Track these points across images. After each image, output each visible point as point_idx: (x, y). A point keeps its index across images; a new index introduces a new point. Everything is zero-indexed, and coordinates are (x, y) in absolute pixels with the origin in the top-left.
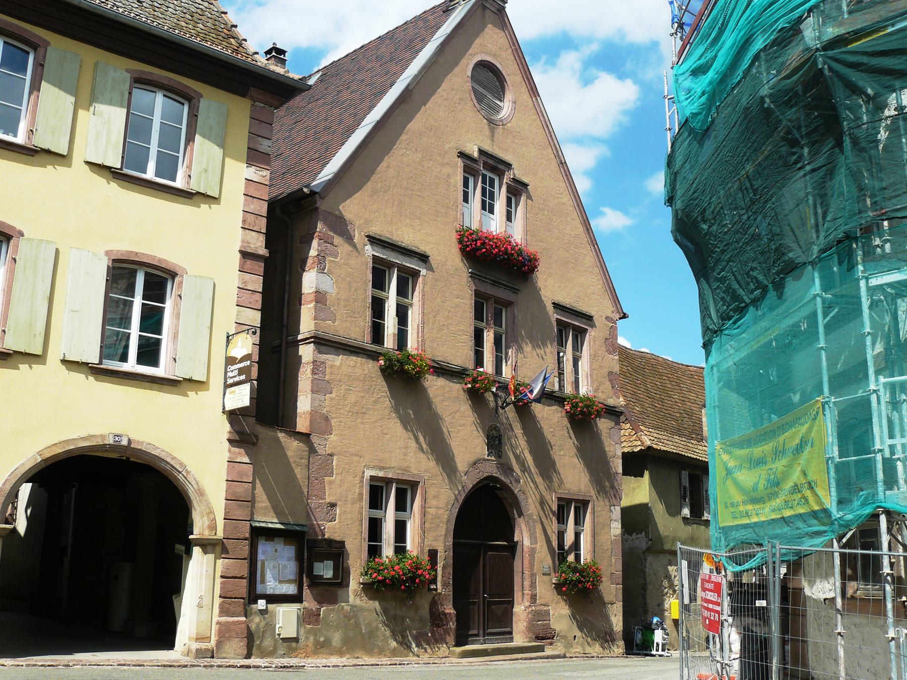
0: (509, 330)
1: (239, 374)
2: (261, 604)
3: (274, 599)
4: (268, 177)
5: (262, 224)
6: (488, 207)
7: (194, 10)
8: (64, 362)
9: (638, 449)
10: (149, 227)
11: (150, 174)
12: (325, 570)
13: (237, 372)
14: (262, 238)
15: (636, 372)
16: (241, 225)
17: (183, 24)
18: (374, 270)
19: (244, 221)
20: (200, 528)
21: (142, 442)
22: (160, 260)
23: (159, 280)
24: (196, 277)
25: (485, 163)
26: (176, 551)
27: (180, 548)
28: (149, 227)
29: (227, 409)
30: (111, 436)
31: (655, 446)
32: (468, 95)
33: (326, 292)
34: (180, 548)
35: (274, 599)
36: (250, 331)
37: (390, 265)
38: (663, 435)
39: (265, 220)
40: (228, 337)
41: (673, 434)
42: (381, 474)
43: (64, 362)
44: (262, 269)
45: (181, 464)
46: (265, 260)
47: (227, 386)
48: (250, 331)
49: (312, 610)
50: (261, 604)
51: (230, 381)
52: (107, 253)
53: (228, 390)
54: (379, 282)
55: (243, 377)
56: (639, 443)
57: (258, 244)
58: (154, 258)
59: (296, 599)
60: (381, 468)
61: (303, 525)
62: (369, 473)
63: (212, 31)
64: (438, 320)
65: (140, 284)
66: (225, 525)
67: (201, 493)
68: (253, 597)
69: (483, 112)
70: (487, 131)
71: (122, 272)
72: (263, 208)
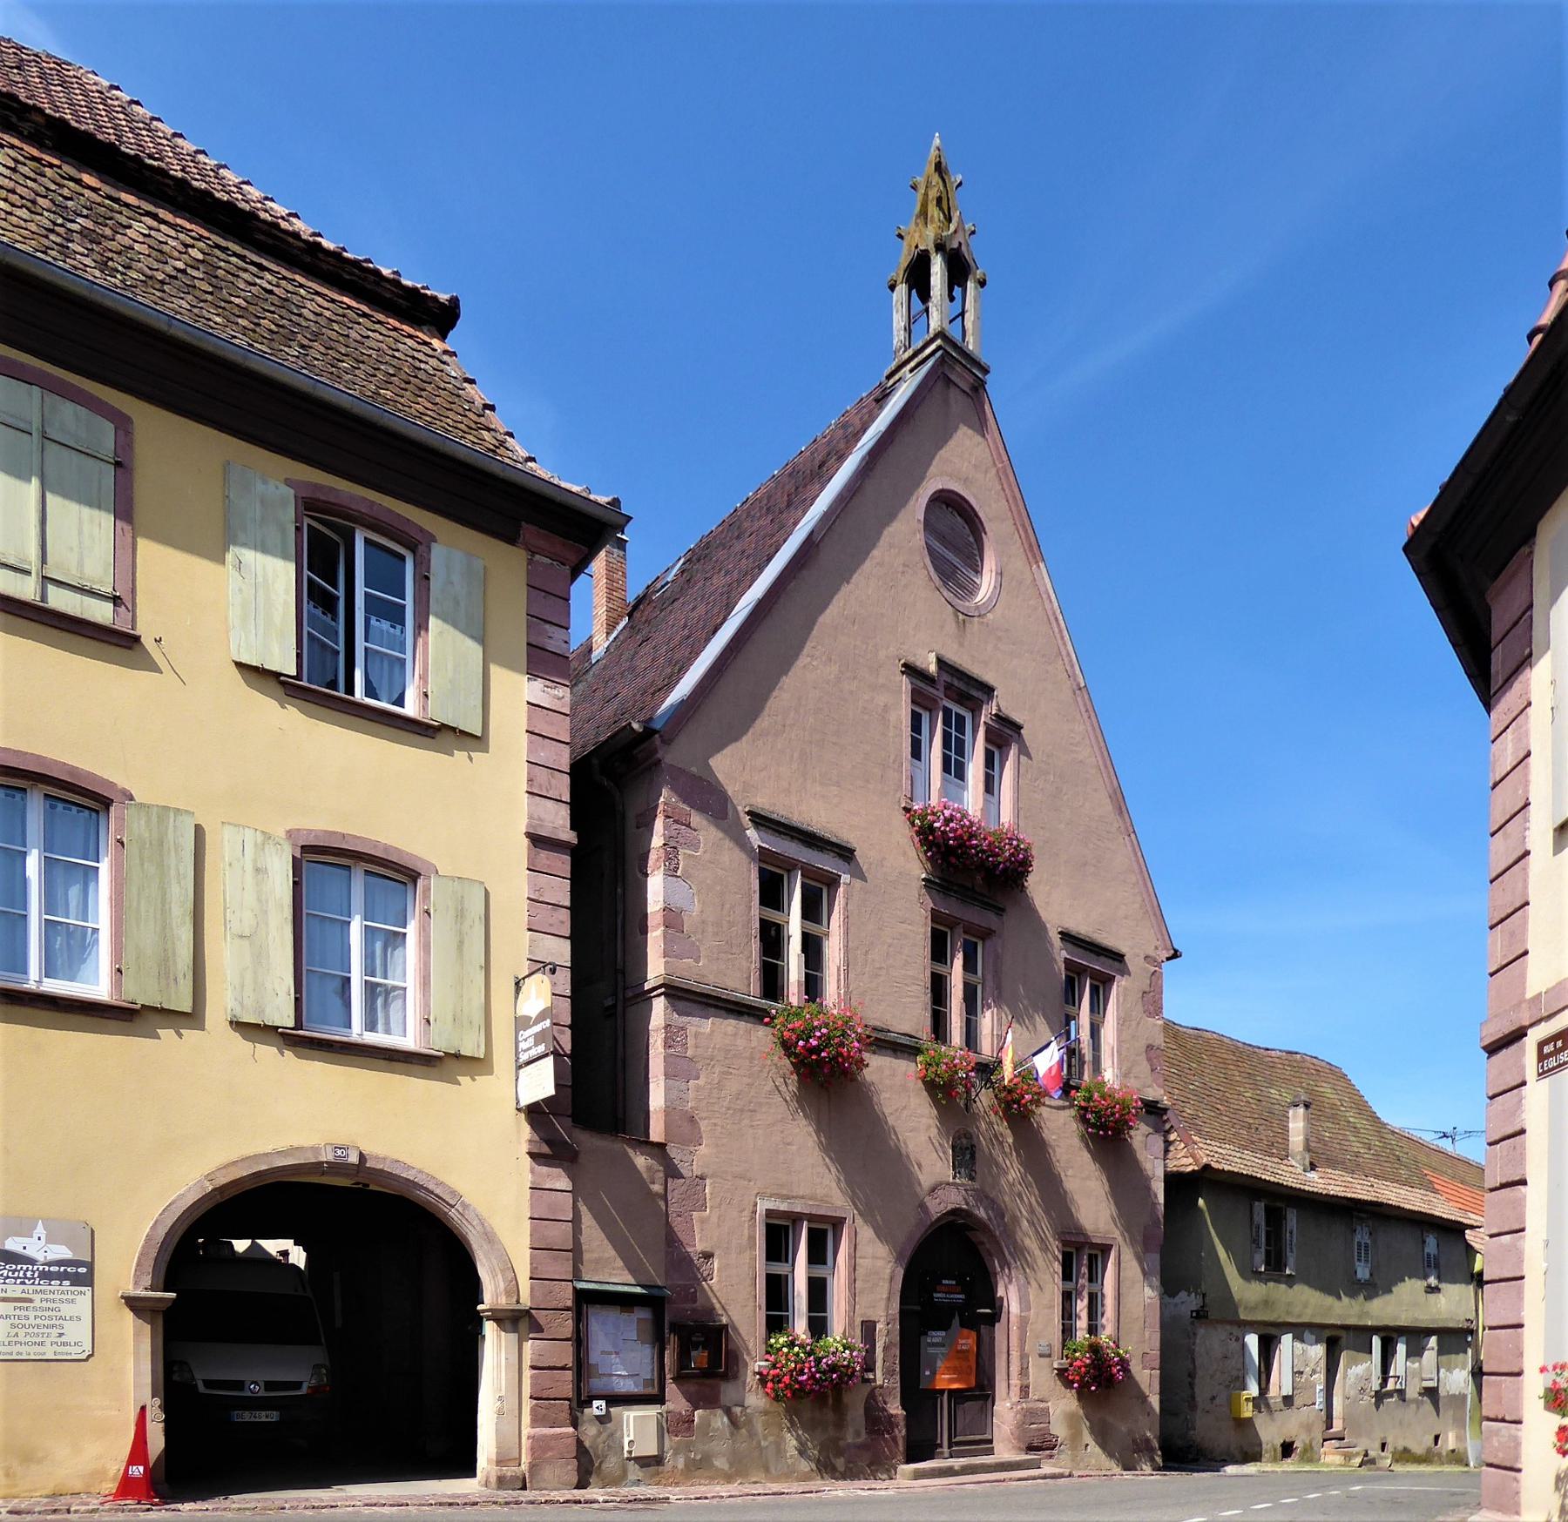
5: (562, 787)
6: (954, 768)
9: (1189, 1169)
13: (532, 1040)
22: (387, 848)
23: (397, 875)
30: (329, 1149)
37: (791, 865)
39: (567, 779)
42: (783, 1207)
45: (453, 1193)
51: (524, 1057)
52: (289, 833)
56: (1191, 1160)
57: (558, 821)
62: (763, 1206)
70: (951, 626)
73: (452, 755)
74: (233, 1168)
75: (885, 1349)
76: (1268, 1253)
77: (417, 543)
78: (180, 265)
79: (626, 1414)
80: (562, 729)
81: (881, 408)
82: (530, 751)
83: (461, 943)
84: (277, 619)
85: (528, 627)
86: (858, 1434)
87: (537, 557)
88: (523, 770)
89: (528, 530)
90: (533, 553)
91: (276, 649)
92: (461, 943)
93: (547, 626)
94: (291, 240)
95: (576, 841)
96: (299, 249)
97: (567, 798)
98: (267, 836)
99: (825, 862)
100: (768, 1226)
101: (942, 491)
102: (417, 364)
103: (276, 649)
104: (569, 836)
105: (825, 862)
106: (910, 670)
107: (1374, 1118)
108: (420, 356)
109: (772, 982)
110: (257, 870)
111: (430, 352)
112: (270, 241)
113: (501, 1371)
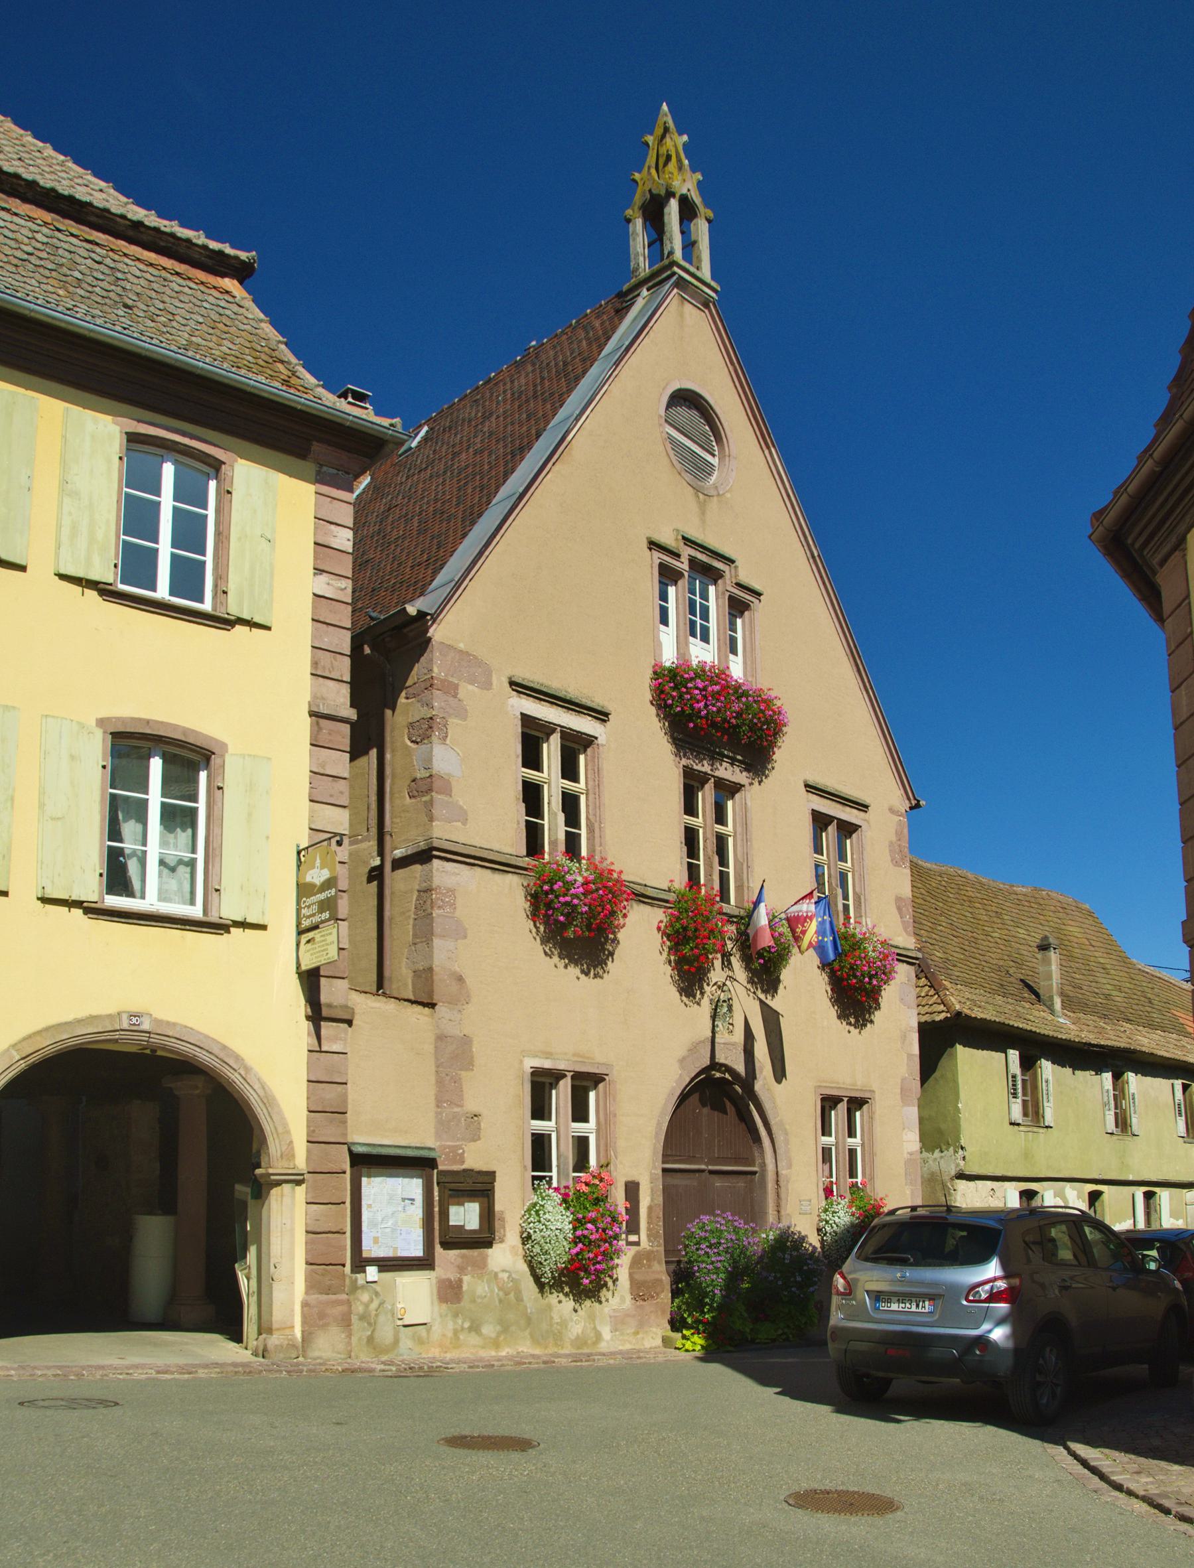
0: (739, 830)
1: (321, 911)
2: (372, 1272)
3: (390, 1265)
4: (350, 590)
5: (344, 667)
6: (696, 629)
7: (216, 317)
8: (512, 684)
9: (942, 1016)
10: (163, 672)
11: (162, 592)
12: (466, 1215)
13: (315, 907)
14: (345, 690)
15: (933, 897)
16: (308, 669)
17: (199, 340)
18: (525, 737)
19: (315, 664)
20: (274, 1163)
21: (174, 1024)
22: (186, 731)
23: (188, 759)
24: (243, 756)
25: (693, 561)
26: (237, 1195)
27: (242, 1190)
28: (163, 672)
29: (304, 968)
30: (125, 1017)
31: (966, 1011)
32: (662, 448)
33: (449, 775)
34: (242, 1190)
35: (390, 1265)
36: (334, 841)
37: (547, 729)
38: (977, 995)
39: (347, 661)
40: (299, 853)
41: (994, 992)
42: (547, 1064)
43: (512, 684)
44: (347, 741)
45: (238, 1058)
46: (354, 726)
47: (300, 933)
48: (334, 841)
49: (449, 1280)
50: (372, 1272)
51: (306, 923)
52: (101, 722)
53: (304, 938)
54: (532, 758)
55: (326, 915)
56: (942, 1007)
57: (339, 699)
58: (175, 727)
59: (424, 1263)
60: (548, 1055)
61: (430, 1149)
62: (530, 1063)
63: (247, 351)
64: (636, 816)
65: (157, 763)
66: (308, 1151)
67: (269, 1101)
68: (360, 1264)
69: (688, 477)
70: (693, 505)
71: (130, 747)
72: (344, 642)
73: (1155, 426)
74: (38, 1038)
75: (650, 1208)
76: (1025, 1102)
77: (216, 466)
78: (29, 249)
79: (399, 1280)
80: (344, 617)
81: (621, 319)
82: (314, 637)
83: (250, 815)
84: (100, 535)
85: (316, 528)
86: (623, 1299)
87: (325, 469)
88: (306, 655)
89: (316, 447)
90: (321, 465)
91: (96, 560)
92: (250, 815)
93: (333, 527)
94: (118, 219)
95: (355, 717)
96: (125, 225)
97: (347, 678)
98: (82, 726)
99: (583, 724)
100: (533, 1082)
101: (680, 390)
102: (221, 311)
103: (96, 560)
104: (352, 714)
105: (583, 724)
106: (653, 545)
107: (1125, 961)
108: (223, 304)
109: (534, 836)
110: (72, 757)
111: (231, 299)
112: (101, 222)
113: (287, 1226)
